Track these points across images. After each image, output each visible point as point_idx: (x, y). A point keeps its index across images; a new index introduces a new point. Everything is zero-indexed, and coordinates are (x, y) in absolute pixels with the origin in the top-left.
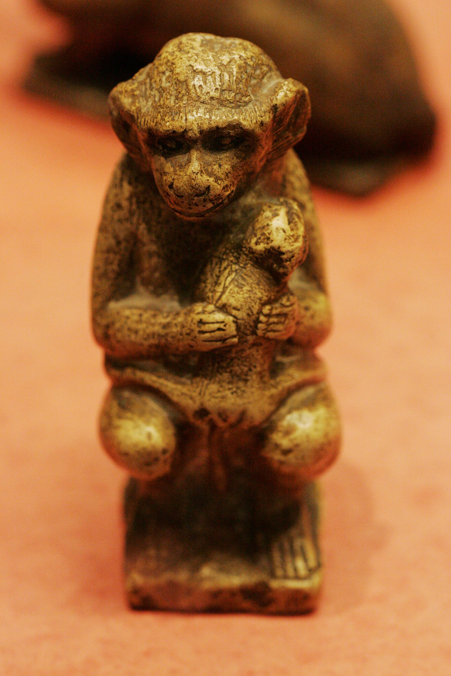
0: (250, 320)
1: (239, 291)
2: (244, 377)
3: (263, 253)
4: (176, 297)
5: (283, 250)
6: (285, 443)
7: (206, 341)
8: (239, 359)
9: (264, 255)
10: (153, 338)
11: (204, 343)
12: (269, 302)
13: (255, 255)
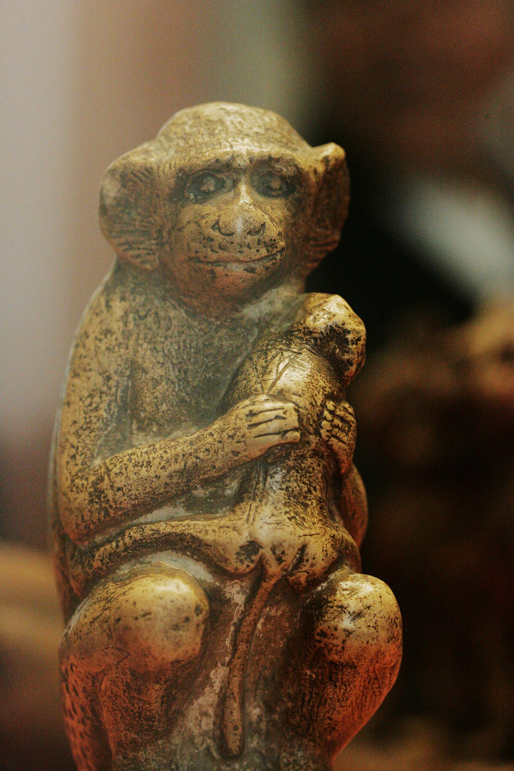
2: (301, 500)
5: (348, 327)
7: (259, 436)
10: (176, 461)
11: (257, 438)
13: (314, 335)
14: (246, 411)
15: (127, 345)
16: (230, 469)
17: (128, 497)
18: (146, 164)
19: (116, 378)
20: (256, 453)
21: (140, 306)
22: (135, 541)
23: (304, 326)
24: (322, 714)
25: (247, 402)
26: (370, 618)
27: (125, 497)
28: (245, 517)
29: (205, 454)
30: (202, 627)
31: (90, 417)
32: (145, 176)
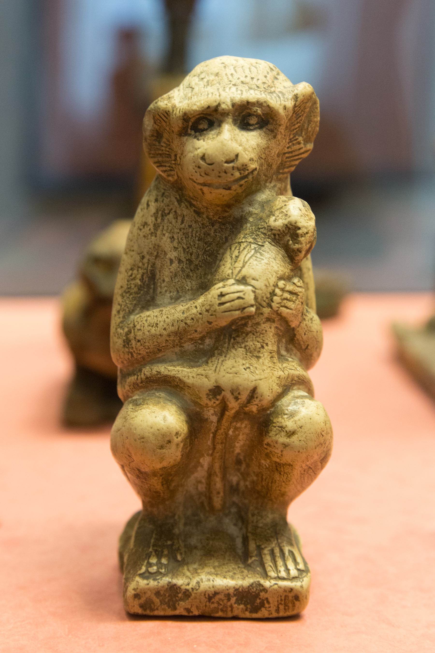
0: (267, 291)
1: (258, 264)
2: (256, 354)
3: (280, 228)
4: (239, 103)
5: (299, 225)
6: (290, 424)
7: (225, 312)
8: (253, 334)
9: (281, 230)
11: (223, 314)
12: (288, 279)
14: (218, 292)
15: (156, 234)
16: (207, 333)
17: (144, 347)
18: (166, 108)
19: (147, 257)
20: (223, 323)
21: (166, 206)
22: (147, 378)
23: (268, 224)
24: (274, 488)
25: (221, 284)
26: (302, 434)
27: (142, 347)
28: (214, 368)
29: (191, 321)
30: (182, 445)
31: (131, 284)
32: (165, 117)
